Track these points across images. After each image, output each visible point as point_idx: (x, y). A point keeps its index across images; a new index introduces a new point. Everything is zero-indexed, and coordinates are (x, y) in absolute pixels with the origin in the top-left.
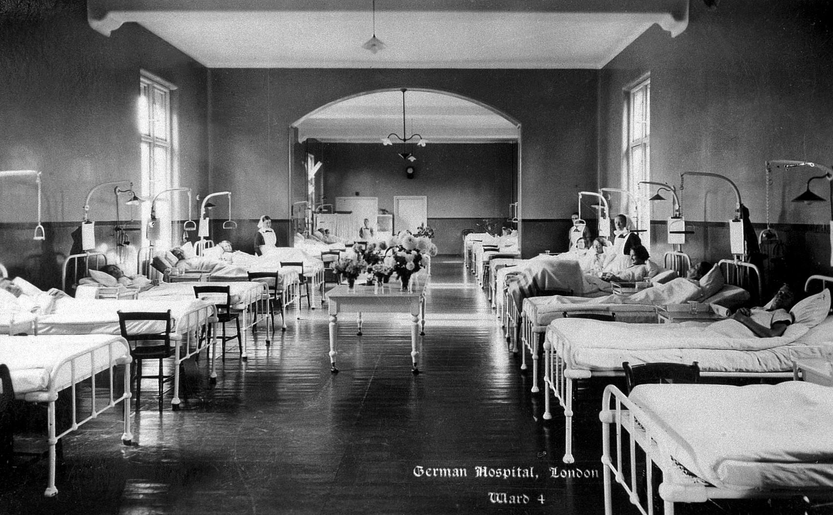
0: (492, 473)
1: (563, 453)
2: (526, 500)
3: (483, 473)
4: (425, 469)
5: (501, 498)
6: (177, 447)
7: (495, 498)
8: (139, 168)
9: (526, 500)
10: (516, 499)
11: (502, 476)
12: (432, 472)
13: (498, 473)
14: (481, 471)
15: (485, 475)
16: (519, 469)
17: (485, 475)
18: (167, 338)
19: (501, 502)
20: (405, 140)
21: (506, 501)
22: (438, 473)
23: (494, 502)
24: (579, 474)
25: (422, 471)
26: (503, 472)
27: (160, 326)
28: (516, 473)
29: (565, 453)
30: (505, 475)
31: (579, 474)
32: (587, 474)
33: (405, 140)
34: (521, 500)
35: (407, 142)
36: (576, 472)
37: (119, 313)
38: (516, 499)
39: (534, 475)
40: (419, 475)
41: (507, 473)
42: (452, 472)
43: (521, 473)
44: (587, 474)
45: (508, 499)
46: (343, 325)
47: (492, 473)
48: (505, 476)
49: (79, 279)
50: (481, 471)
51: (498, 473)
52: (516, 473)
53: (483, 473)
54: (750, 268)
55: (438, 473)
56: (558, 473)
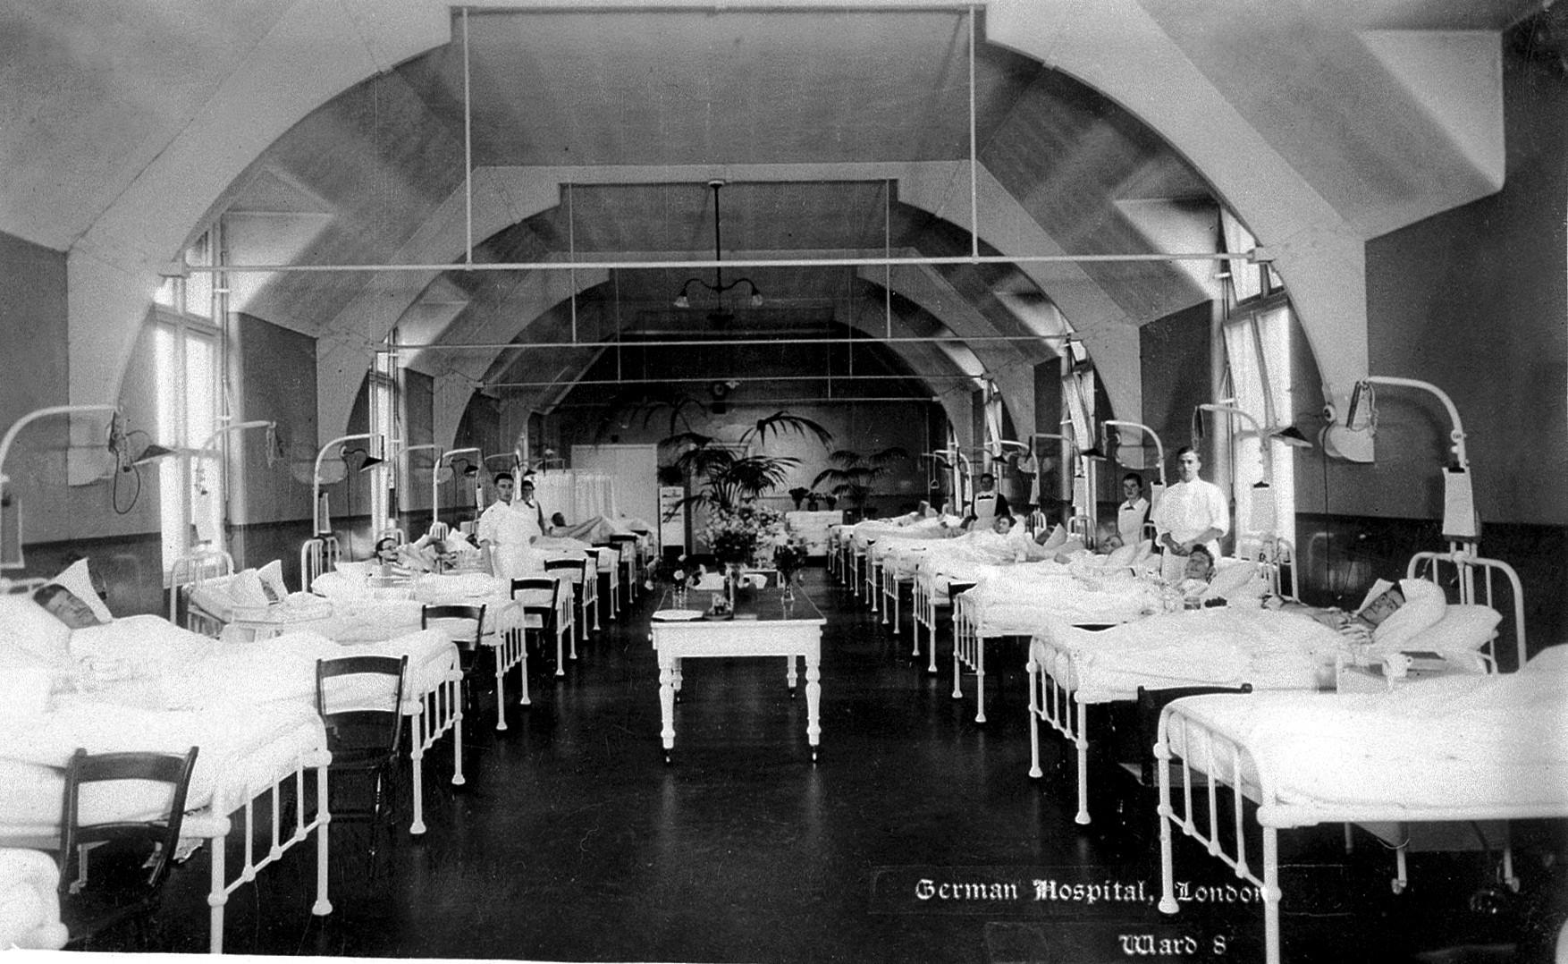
0: (1065, 892)
2: (1191, 947)
3: (1049, 893)
4: (936, 886)
5: (1145, 945)
6: (1081, 138)
8: (254, 836)
9: (1191, 947)
11: (1085, 898)
12: (949, 891)
13: (1078, 892)
14: (1042, 889)
15: (1053, 896)
16: (1117, 887)
17: (1053, 896)
21: (1152, 950)
22: (962, 892)
23: (1130, 952)
24: (1232, 895)
26: (1086, 891)
28: (1112, 892)
29: (226, 907)
30: (1091, 898)
31: (1232, 895)
34: (1181, 947)
36: (1225, 891)
38: (1172, 945)
40: (926, 897)
41: (1095, 893)
42: (988, 891)
43: (1122, 892)
45: (1157, 947)
47: (1065, 892)
48: (1091, 898)
51: (1078, 892)
52: (1112, 892)
53: (1049, 893)
54: (1495, 570)
55: (962, 892)
56: (1191, 893)
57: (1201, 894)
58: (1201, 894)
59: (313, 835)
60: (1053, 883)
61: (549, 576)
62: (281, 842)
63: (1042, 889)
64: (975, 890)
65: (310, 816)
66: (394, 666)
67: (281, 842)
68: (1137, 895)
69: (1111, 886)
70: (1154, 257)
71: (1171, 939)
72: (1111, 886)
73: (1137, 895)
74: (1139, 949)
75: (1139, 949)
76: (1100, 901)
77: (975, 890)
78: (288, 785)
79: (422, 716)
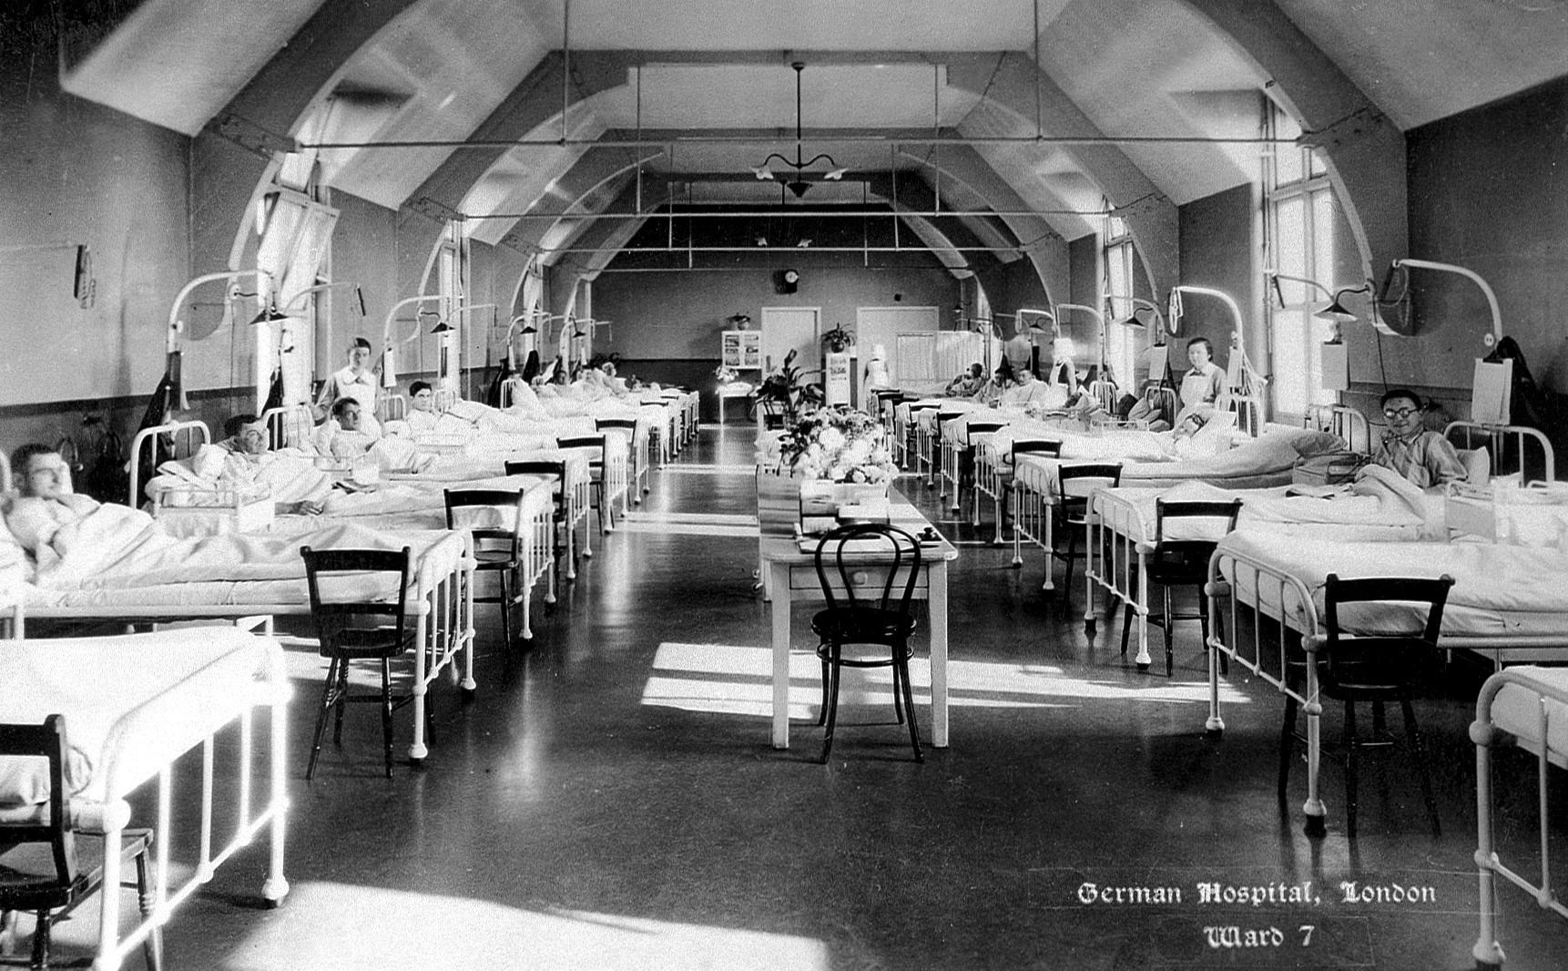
0: (1229, 894)
1: (412, 740)
2: (1277, 938)
3: (1213, 896)
7: (1220, 938)
9: (1277, 938)
10: (1258, 937)
11: (1250, 902)
12: (1113, 895)
16: (1282, 888)
17: (1218, 899)
18: (398, 610)
19: (1229, 944)
20: (799, 165)
21: (1238, 943)
24: (1399, 895)
25: (1095, 893)
26: (1251, 894)
27: (384, 584)
31: (1399, 895)
32: (1413, 894)
33: (799, 165)
34: (1268, 938)
35: (804, 169)
36: (1392, 890)
37: (305, 552)
38: (1258, 937)
39: (1313, 896)
41: (1260, 896)
42: (1152, 895)
44: (1413, 894)
45: (1242, 938)
46: (1423, 832)
47: (1229, 894)
48: (1256, 901)
49: (158, 464)
50: (1207, 891)
53: (1213, 896)
54: (1526, 436)
56: (1358, 892)
57: (1368, 894)
58: (1368, 894)
59: (264, 838)
60: (1217, 886)
61: (557, 455)
62: (213, 857)
63: (1207, 891)
64: (1140, 894)
65: (261, 796)
66: (397, 561)
67: (213, 857)
68: (1303, 895)
69: (1276, 887)
70: (962, 142)
71: (1257, 930)
72: (1276, 887)
73: (1303, 895)
74: (1224, 942)
75: (1224, 942)
76: (1266, 903)
77: (1140, 894)
78: (226, 743)
79: (429, 617)
